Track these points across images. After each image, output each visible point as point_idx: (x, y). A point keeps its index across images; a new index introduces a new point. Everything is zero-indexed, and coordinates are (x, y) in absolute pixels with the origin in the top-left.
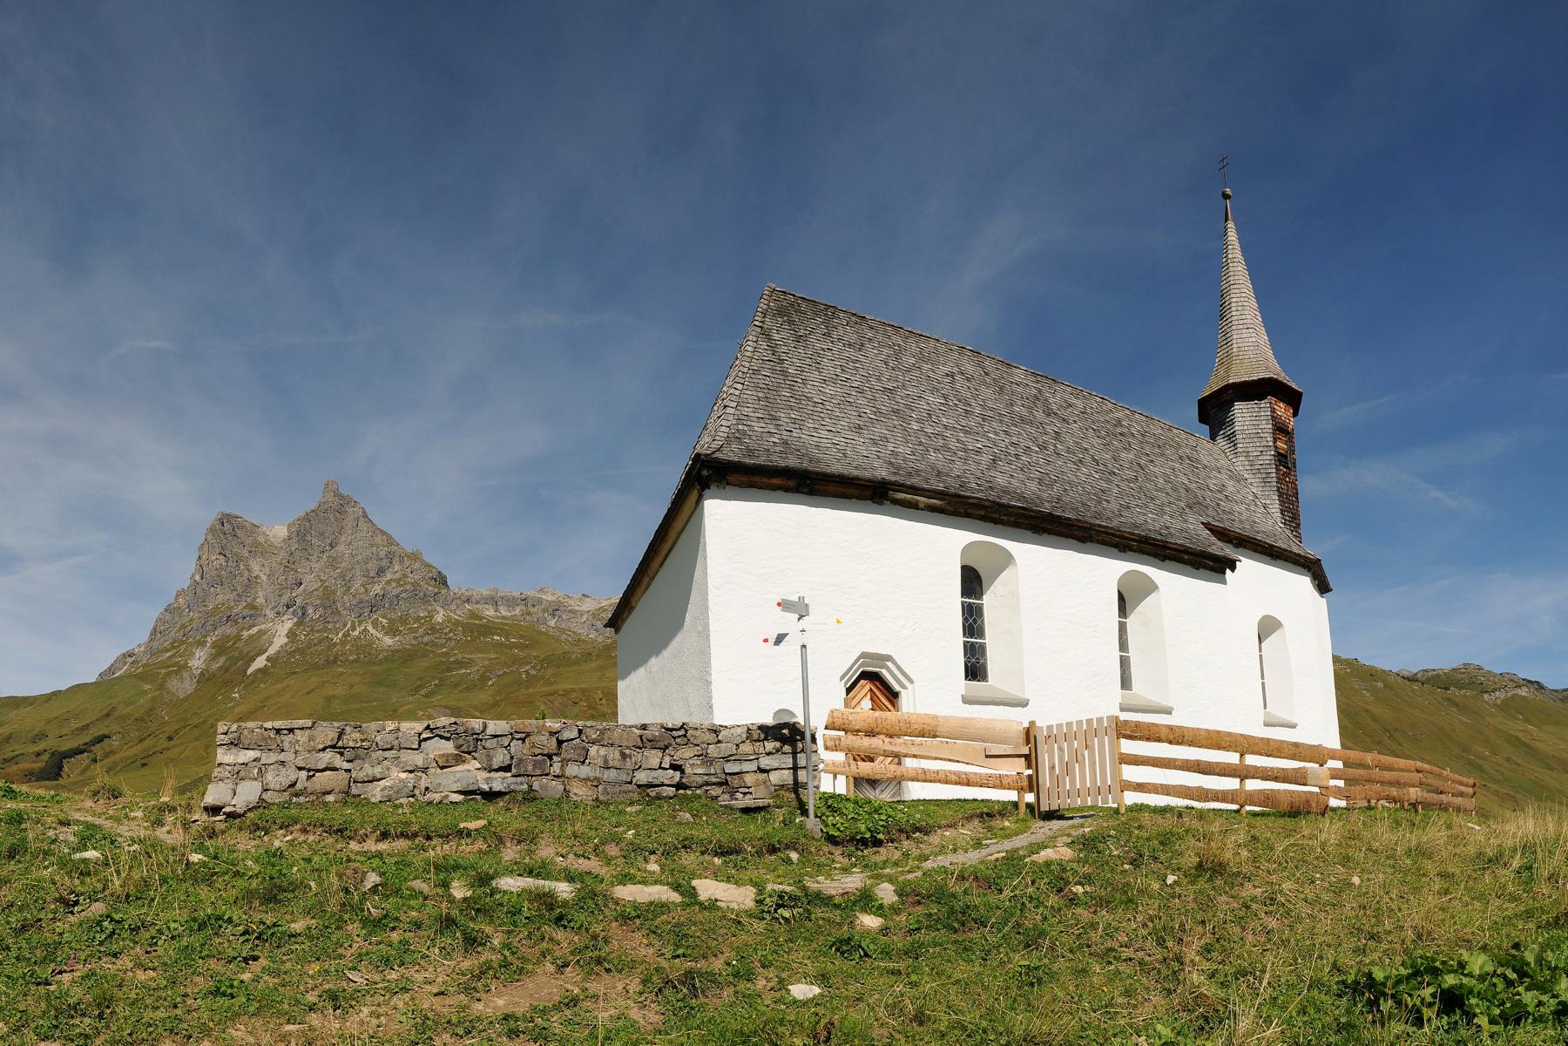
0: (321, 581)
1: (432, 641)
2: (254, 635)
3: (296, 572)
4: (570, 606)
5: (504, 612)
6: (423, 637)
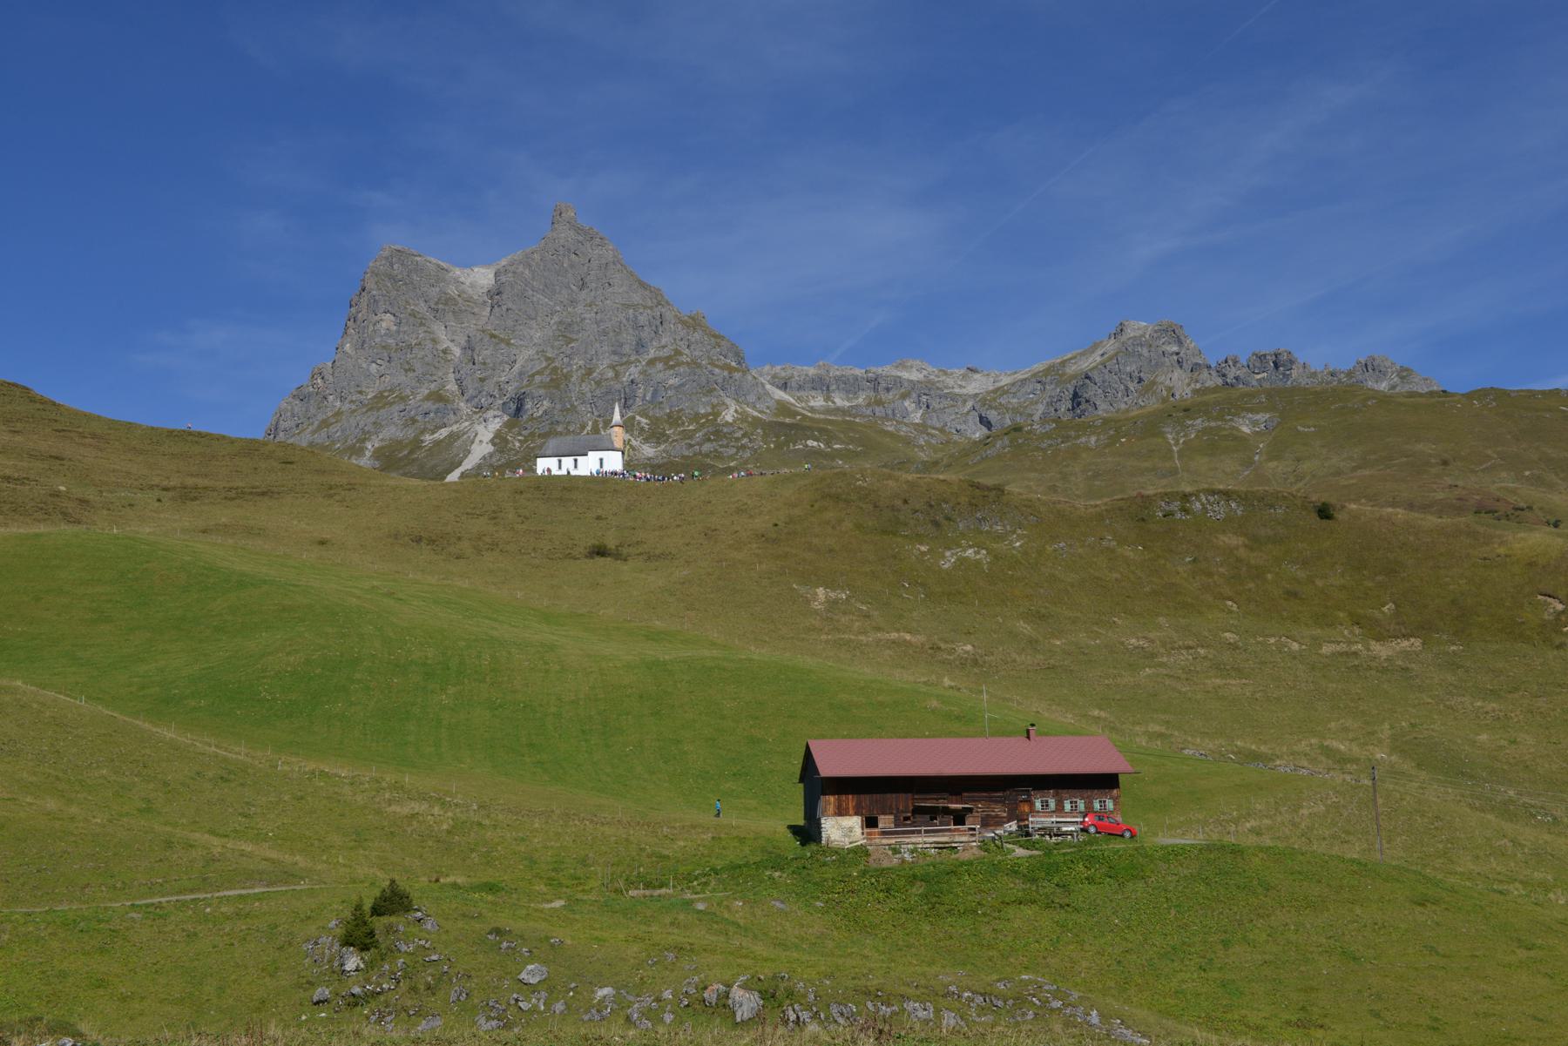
0: (548, 359)
1: (716, 450)
2: (441, 441)
3: (508, 344)
4: (946, 387)
5: (840, 401)
6: (700, 444)
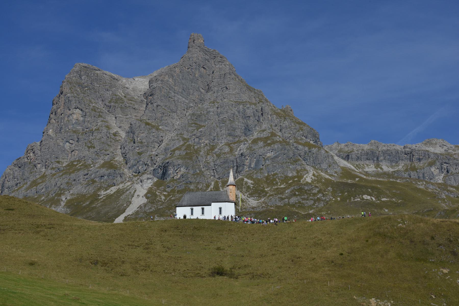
0: (184, 139)
1: (300, 202)
2: (112, 195)
3: (158, 129)
5: (386, 168)
